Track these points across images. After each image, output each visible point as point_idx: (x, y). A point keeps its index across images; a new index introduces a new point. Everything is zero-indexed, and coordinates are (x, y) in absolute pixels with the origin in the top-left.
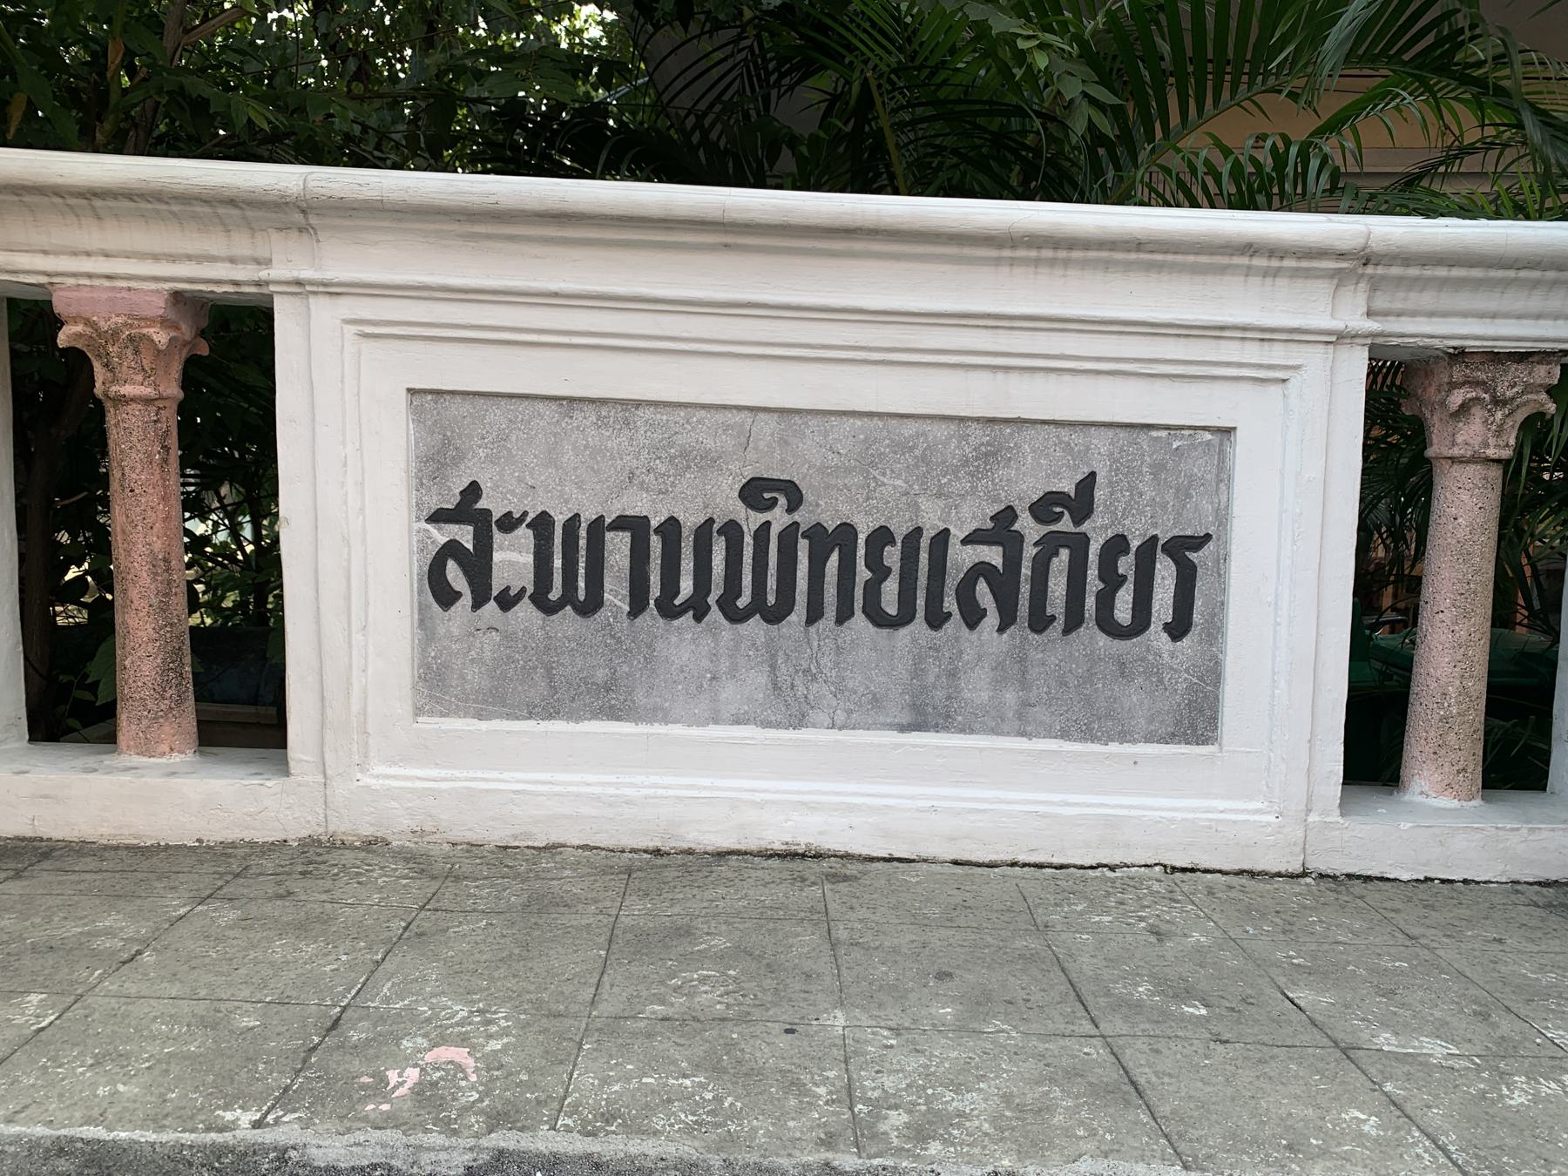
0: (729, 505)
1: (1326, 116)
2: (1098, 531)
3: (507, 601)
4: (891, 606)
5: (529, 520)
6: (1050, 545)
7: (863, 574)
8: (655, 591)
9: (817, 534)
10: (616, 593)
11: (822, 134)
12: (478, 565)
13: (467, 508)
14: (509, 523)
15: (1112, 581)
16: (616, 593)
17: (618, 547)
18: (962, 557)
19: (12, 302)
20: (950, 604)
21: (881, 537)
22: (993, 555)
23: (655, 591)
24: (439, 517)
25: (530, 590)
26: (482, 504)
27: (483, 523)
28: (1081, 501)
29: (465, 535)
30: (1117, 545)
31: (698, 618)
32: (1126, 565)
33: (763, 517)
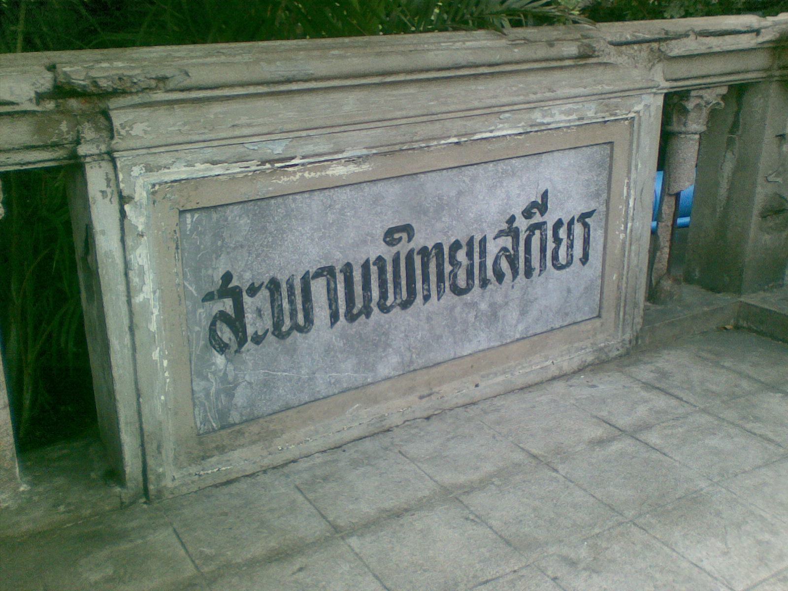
0: (379, 249)
1: (773, 572)
2: (550, 219)
3: (258, 340)
4: (462, 282)
5: (265, 284)
6: (532, 229)
7: (448, 268)
8: (342, 310)
9: (424, 252)
10: (321, 313)
11: (13, 28)
12: (236, 322)
13: (227, 289)
14: (253, 291)
15: (558, 241)
16: (321, 313)
17: (319, 288)
18: (493, 248)
19: (5, 176)
20: (490, 273)
21: (456, 246)
22: (507, 242)
23: (342, 310)
24: (209, 297)
25: (271, 329)
26: (234, 283)
27: (236, 295)
28: (541, 205)
29: (227, 305)
30: (559, 224)
31: (368, 316)
32: (563, 233)
33: (394, 250)
